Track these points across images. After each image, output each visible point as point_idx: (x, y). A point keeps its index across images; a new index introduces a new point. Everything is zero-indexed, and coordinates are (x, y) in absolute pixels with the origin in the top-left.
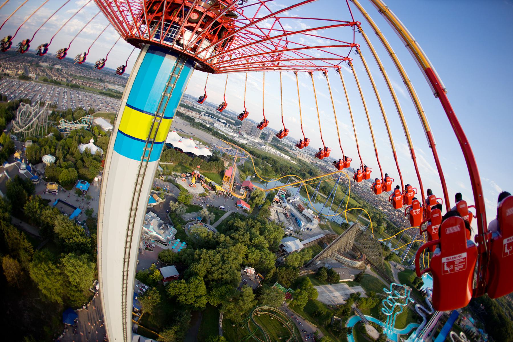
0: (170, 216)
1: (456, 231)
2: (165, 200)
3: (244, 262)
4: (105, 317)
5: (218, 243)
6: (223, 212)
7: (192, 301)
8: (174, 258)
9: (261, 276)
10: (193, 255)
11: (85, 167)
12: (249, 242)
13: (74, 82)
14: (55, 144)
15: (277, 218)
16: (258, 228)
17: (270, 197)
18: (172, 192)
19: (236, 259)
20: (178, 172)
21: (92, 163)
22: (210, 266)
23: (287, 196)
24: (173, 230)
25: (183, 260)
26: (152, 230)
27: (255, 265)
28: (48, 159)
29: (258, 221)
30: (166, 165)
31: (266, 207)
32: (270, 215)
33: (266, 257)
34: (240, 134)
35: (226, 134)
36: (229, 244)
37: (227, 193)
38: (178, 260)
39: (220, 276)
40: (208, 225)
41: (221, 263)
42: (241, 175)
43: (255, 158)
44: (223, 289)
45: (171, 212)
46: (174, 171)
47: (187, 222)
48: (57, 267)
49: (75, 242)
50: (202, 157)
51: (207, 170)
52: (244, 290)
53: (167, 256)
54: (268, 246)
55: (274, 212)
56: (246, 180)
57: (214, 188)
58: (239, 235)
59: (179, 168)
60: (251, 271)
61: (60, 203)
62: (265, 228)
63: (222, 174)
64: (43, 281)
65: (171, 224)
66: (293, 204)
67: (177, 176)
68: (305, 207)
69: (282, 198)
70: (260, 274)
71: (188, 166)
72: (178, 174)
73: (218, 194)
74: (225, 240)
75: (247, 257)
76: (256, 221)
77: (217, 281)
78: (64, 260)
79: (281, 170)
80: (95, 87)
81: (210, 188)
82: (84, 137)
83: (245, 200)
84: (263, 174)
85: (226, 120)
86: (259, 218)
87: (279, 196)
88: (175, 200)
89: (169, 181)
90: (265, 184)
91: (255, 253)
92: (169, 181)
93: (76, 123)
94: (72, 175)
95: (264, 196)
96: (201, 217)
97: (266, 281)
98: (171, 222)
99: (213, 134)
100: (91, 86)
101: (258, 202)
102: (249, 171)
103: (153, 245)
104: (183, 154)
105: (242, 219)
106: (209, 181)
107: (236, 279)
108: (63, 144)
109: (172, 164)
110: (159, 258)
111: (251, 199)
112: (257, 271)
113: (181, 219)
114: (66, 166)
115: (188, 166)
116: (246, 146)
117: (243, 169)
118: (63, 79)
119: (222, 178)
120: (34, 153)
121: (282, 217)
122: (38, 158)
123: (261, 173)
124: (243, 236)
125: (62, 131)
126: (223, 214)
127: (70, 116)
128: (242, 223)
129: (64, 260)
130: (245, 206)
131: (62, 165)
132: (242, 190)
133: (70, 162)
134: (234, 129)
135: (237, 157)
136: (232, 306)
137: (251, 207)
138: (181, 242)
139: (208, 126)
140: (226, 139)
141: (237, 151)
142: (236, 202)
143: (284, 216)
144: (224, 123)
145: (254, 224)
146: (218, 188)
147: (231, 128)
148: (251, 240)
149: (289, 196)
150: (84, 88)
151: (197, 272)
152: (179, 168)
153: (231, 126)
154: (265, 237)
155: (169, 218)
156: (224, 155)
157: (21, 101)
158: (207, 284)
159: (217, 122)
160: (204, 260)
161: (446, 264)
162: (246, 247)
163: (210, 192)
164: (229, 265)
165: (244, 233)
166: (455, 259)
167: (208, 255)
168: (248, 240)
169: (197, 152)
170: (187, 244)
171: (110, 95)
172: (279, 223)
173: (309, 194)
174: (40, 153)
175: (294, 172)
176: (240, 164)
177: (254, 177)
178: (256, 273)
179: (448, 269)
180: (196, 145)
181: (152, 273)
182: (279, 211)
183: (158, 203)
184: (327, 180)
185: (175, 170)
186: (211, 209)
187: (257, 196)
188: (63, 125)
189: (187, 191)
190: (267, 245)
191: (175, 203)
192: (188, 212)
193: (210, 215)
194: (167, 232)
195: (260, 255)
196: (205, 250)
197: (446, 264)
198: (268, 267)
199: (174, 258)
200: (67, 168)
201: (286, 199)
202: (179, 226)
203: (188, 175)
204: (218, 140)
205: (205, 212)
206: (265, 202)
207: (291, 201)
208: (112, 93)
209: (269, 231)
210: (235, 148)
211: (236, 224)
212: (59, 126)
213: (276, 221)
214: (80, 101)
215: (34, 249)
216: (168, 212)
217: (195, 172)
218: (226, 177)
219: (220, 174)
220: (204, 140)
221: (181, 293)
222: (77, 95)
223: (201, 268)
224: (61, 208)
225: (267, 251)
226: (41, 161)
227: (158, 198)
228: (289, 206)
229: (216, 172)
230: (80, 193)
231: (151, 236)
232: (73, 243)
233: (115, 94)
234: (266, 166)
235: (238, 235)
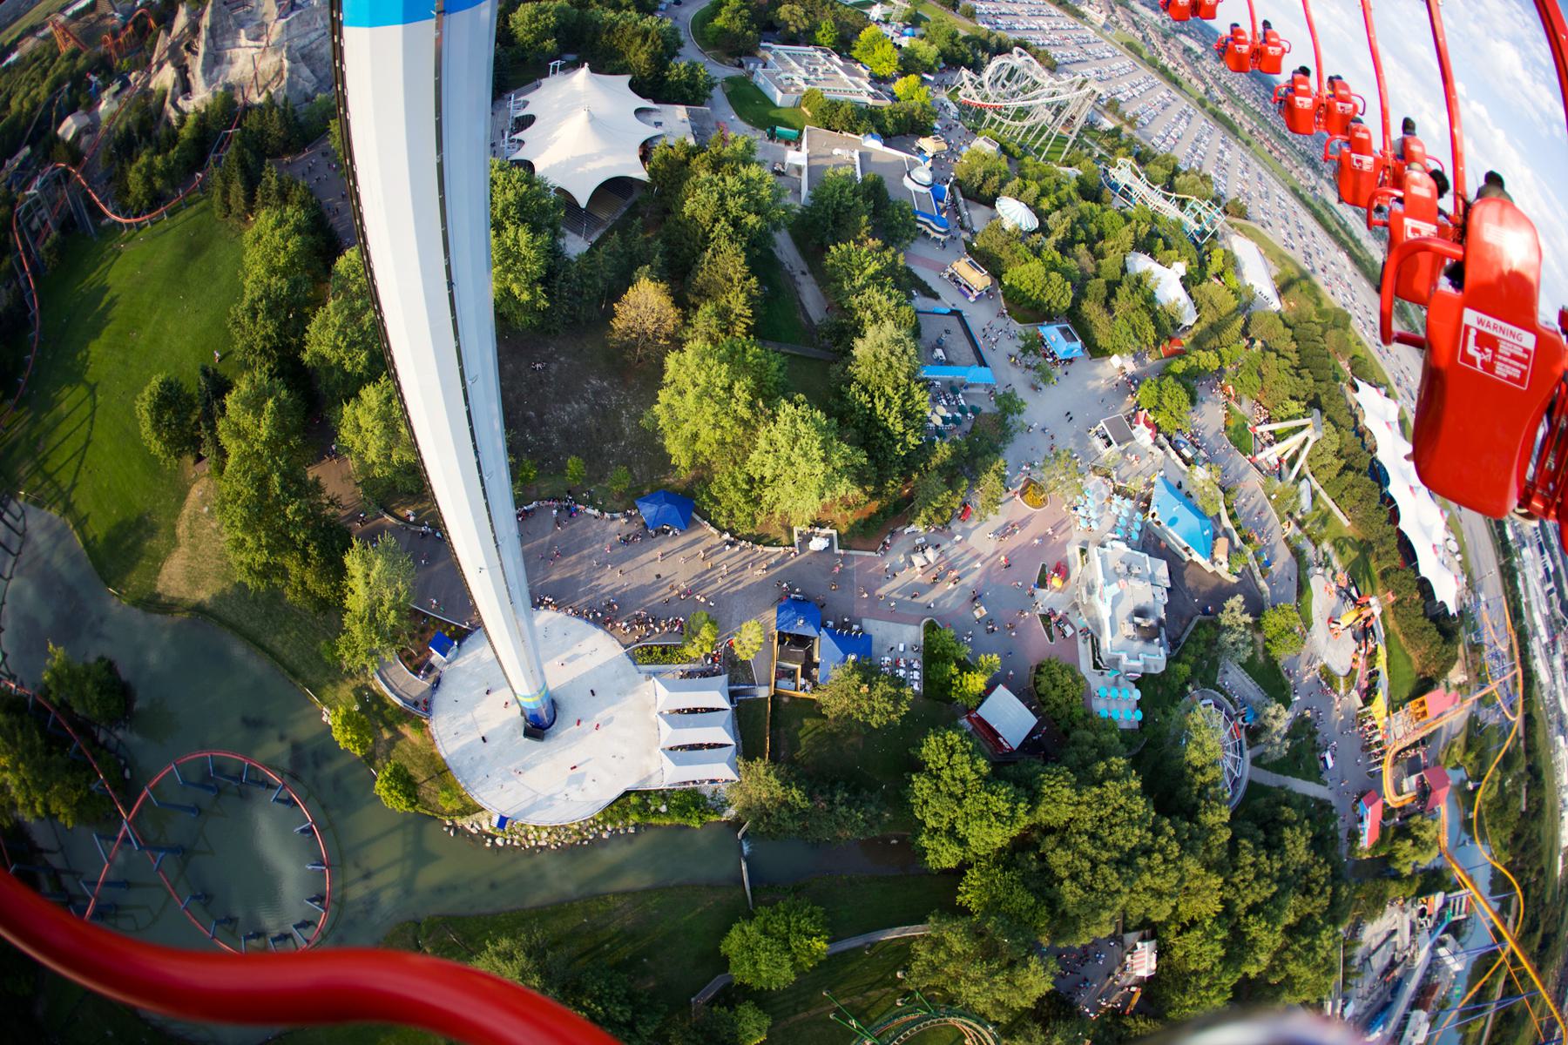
0: (1200, 625)
2: (1234, 580)
3: (1164, 925)
5: (1191, 813)
6: (1315, 773)
7: (931, 823)
8: (1066, 709)
9: (1135, 1001)
10: (1103, 755)
11: (1108, 308)
12: (1241, 907)
13: (1226, 110)
14: (1065, 199)
15: (1373, 947)
16: (1308, 910)
17: (1433, 880)
18: (1270, 584)
19: (1159, 894)
20: (1341, 560)
21: (1133, 316)
22: (1088, 826)
23: (1455, 929)
24: (1156, 658)
25: (1072, 735)
26: (1109, 600)
27: (1169, 966)
28: (1014, 213)
29: (1335, 893)
30: (1330, 512)
31: (1394, 889)
32: (1372, 917)
33: (1208, 988)
34: (1554, 642)
35: (1528, 605)
36: (1208, 850)
37: (1379, 744)
38: (1064, 724)
39: (1064, 873)
40: (1247, 754)
41: (1116, 854)
42: (1453, 744)
43: (1522, 744)
44: (1023, 899)
45: (1212, 623)
46: (1334, 544)
47: (1217, 688)
48: (751, 405)
49: (873, 409)
50: (1425, 587)
51: (1405, 635)
52: (1033, 966)
53: (1055, 686)
54: (1252, 975)
55: (1391, 926)
56: (1448, 770)
57: (1368, 696)
58: (1253, 865)
59: (1352, 554)
60: (1144, 962)
61: (954, 320)
62: (1315, 932)
63: (1425, 685)
64: (681, 393)
65: (1173, 643)
66: (1434, 964)
67: (1328, 564)
68: (1432, 1006)
69: (1441, 916)
70: (1138, 995)
71: (1376, 573)
72: (1335, 561)
73: (1359, 719)
74: (1212, 830)
75: (1185, 928)
76: (1329, 889)
77: (1046, 871)
78: (786, 409)
79: (1524, 849)
80: (1285, 164)
81: (1365, 685)
82: (1168, 247)
83: (1388, 812)
84: (1490, 804)
85: (1557, 569)
86: (1344, 891)
87: (1446, 904)
88: (1256, 607)
89: (1297, 554)
90: (1464, 836)
91: (1207, 947)
92: (1297, 554)
93: (1167, 198)
94: (1050, 295)
95: (1427, 860)
96: (1256, 716)
97: (1119, 1024)
98: (1183, 640)
99: (1501, 568)
100: (1275, 154)
101: (1400, 855)
102: (1477, 757)
103: (1069, 631)
104: (1389, 528)
105: (1321, 843)
106: (1381, 664)
107: (1078, 928)
108: (1087, 212)
109: (1347, 523)
110: (1039, 669)
111: (1400, 826)
112: (1145, 983)
113: (1214, 665)
114: (1053, 262)
115: (1376, 573)
116: (1536, 688)
117: (1475, 733)
118: (1195, 81)
119: (1411, 698)
120: (979, 171)
121: (1378, 962)
122: (987, 191)
123: (1489, 798)
124: (1257, 878)
125: (1115, 186)
126: (1307, 777)
127: (1161, 173)
128: (1301, 849)
129: (786, 409)
130: (1367, 824)
131: (1045, 254)
132: (1414, 778)
133: (1071, 263)
134: (1552, 613)
135: (1493, 686)
136: (958, 948)
137: (1376, 846)
138: (1139, 704)
139: (1510, 535)
140: (1516, 614)
141: (1508, 677)
142: (1369, 790)
143: (1386, 962)
144: (1546, 570)
145: (1317, 890)
146: (1380, 703)
147: (1550, 604)
148: (1254, 909)
149: (1457, 936)
150: (1248, 143)
151: (1043, 795)
152: (1352, 554)
153: (1554, 595)
154: (1286, 948)
155: (1191, 627)
156: (1476, 648)
157: (1024, 45)
158: (1022, 844)
159: (1536, 549)
160: (1101, 797)
162: (1219, 908)
163: (1354, 693)
164: (1119, 885)
165: (1269, 876)
167: (1122, 800)
168: (1249, 901)
169: (1428, 566)
170: (1142, 723)
171: (1318, 217)
172: (1357, 961)
173: (1482, 988)
174: (1002, 184)
175: (1532, 891)
176: (1483, 714)
177: (1470, 786)
178: (1141, 982)
180: (1439, 542)
181: (966, 667)
182: (1396, 938)
183: (1210, 568)
184: (1533, 1015)
185: (1339, 544)
186: (1303, 730)
187: (1416, 840)
188: (1123, 173)
189: (1308, 623)
190: (1253, 971)
191: (1245, 612)
192: (1248, 666)
193: (1278, 740)
194: (1138, 645)
195: (1207, 964)
196: (1136, 784)
198: (1171, 1009)
199: (1066, 709)
200: (1052, 267)
201: (1444, 932)
202: (1184, 669)
203: (1353, 591)
204: (1501, 592)
205: (1280, 719)
206: (1410, 878)
207: (1442, 951)
208: (1327, 216)
209: (1311, 948)
210: (1512, 659)
211: (1287, 833)
212: (1111, 171)
213: (1359, 951)
214: (1223, 167)
215: (749, 330)
216: (1205, 612)
217: (1373, 601)
218: (1423, 703)
219: (1420, 682)
220: (1471, 556)
221: (938, 777)
222: (1222, 146)
223: (1061, 802)
224: (947, 332)
225: (1229, 980)
226: (990, 202)
227: (1221, 556)
228: (1422, 957)
229: (1417, 664)
230: (1035, 346)
231: (1091, 606)
232: (862, 407)
233: (1335, 227)
234: (1517, 795)
235: (1250, 859)
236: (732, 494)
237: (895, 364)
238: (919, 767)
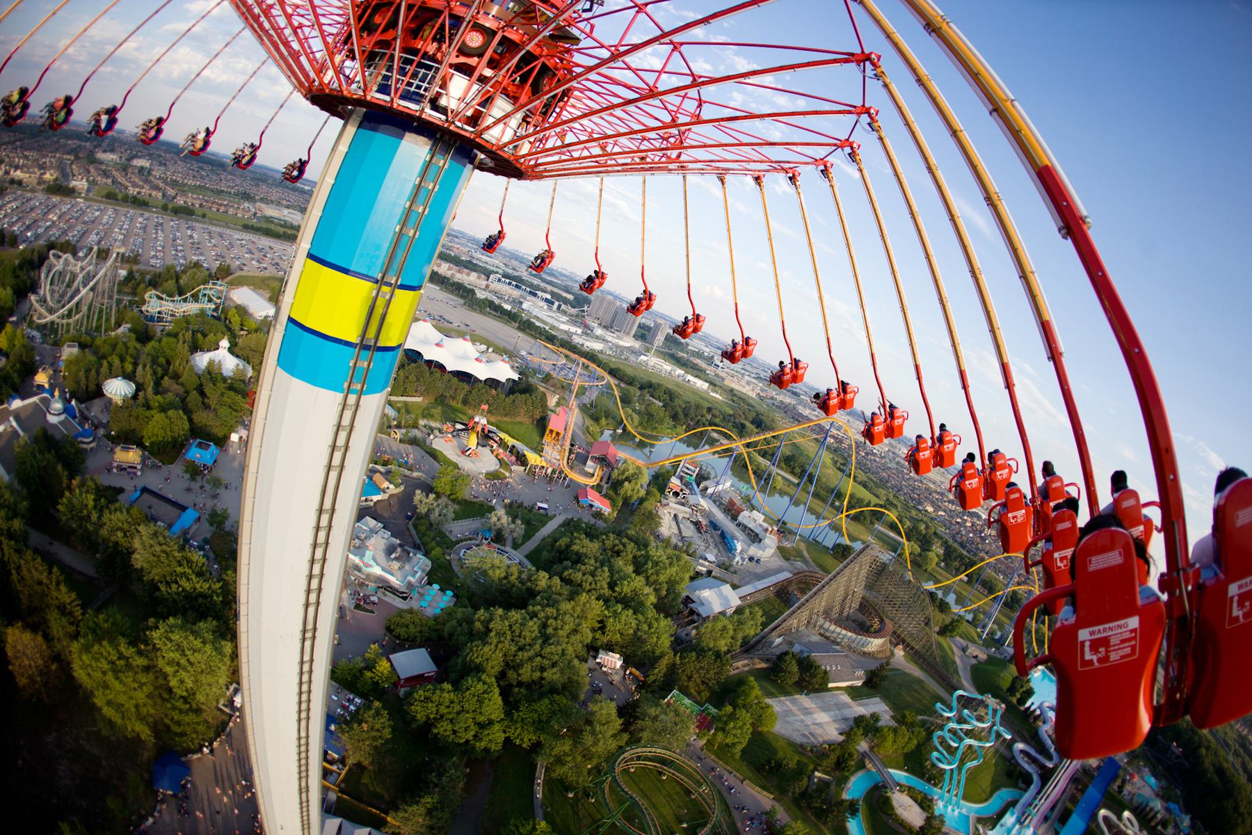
0: (415, 526)
2: (402, 488)
3: (594, 639)
4: (256, 774)
5: (532, 594)
6: (545, 517)
7: (470, 735)
8: (426, 629)
9: (637, 673)
10: (470, 622)
11: (207, 407)
12: (607, 592)
13: (180, 201)
14: (135, 352)
15: (676, 531)
16: (630, 556)
17: (660, 481)
18: (419, 470)
19: (575, 631)
20: (435, 420)
21: (225, 399)
22: (514, 648)
23: (701, 478)
24: (421, 563)
25: (446, 634)
26: (372, 563)
27: (622, 647)
29: (630, 539)
30: (406, 403)
31: (648, 505)
32: (658, 524)
33: (650, 626)
34: (586, 326)
35: (553, 327)
36: (560, 595)
37: (554, 472)
38: (434, 636)
39: (538, 674)
40: (508, 549)
41: (540, 641)
42: (587, 428)
43: (623, 385)
44: (544, 705)
45: (418, 518)
46: (424, 417)
47: (458, 542)
48: (140, 653)
49: (184, 590)
50: (492, 383)
51: (506, 415)
52: (596, 709)
53: (407, 626)
54: (655, 601)
55: (670, 518)
56: (601, 439)
57: (522, 460)
58: (584, 574)
59: (437, 411)
60: (613, 661)
62: (647, 557)
63: (542, 424)
64: (106, 686)
65: (417, 547)
66: (716, 499)
67: (432, 429)
68: (743, 506)
69: (687, 484)
70: (634, 670)
71: (459, 406)
72: (433, 424)
73: (532, 473)
74: (550, 587)
75: (602, 628)
76: (625, 540)
77: (530, 686)
78: (155, 635)
79: (686, 416)
80: (231, 211)
81: (514, 458)
82: (205, 335)
83: (598, 488)
84: (641, 424)
85: (552, 293)
86: (631, 532)
87: (681, 478)
88: (428, 489)
89: (414, 442)
90: (647, 450)
91: (623, 618)
92: (414, 442)
93: (185, 300)
94: (176, 428)
95: (645, 479)
96: (490, 530)
97: (649, 686)
98: (418, 542)
99: (519, 328)
100: (222, 209)
101: (629, 493)
102: (607, 417)
103: (374, 599)
104: (446, 377)
105: (591, 534)
106: (511, 441)
107: (577, 682)
108: (153, 352)
109: (420, 399)
110: (389, 629)
111: (613, 485)
112: (627, 663)
113: (442, 535)
114: (160, 405)
115: (459, 406)
116: (600, 356)
117: (594, 413)
118: (154, 193)
119: (542, 436)
121: (689, 531)
123: (636, 423)
124: (593, 576)
125: (152, 319)
126: (544, 524)
127: (171, 284)
128: (591, 545)
129: (155, 635)
130: (597, 504)
131: (151, 403)
132: (589, 463)
133: (170, 396)
134: (571, 315)
135: (577, 383)
136: (567, 748)
137: (613, 505)
138: (442, 590)
139: (507, 307)
140: (551, 339)
141: (579, 370)
142: (577, 493)
143: (692, 527)
144: (547, 300)
145: (621, 547)
146: (532, 458)
147: (565, 313)
148: (612, 586)
149: (706, 479)
150: (204, 216)
151: (480, 664)
152: (437, 411)
153: (563, 307)
154: (647, 578)
155: (413, 532)
156: (547, 378)
157: (52, 246)
158: (505, 693)
159: (530, 298)
160: (498, 634)
161: (1087, 644)
162: (601, 602)
163: (514, 468)
164: (560, 648)
165: (596, 569)
166: (1111, 633)
167: (507, 623)
168: (606, 586)
169: (481, 372)
170: (455, 595)
171: (268, 233)
172: (680, 544)
173: (754, 473)
175: (717, 420)
176: (586, 400)
177: (620, 431)
178: (625, 666)
179: (1095, 658)
180: (477, 355)
181: (370, 666)
182: (680, 516)
183: (386, 496)
184: (799, 440)
185: (427, 414)
186: (514, 510)
187: (628, 479)
188: (154, 304)
189: (456, 466)
190: (653, 599)
191: (427, 496)
192: (458, 517)
193: (513, 526)
194: (407, 567)
195: (634, 623)
196: (500, 611)
197: (1087, 644)
198: (653, 652)
199: (426, 629)
200: (163, 409)
201: (698, 485)
202: (437, 551)
203: (459, 426)
204: (532, 341)
205: (500, 517)
206: (648, 493)
207: (710, 491)
208: (272, 227)
209: (656, 564)
210: (573, 361)
211: (575, 548)
212: (144, 309)
213: (674, 540)
214: (196, 247)
216: (409, 518)
217: (477, 419)
218: (551, 431)
219: (537, 425)
220: (497, 342)
221: (442, 716)
222: (189, 232)
223: (491, 655)
225: (651, 613)
227: (386, 484)
228: (705, 504)
229: (526, 421)
230: (195, 471)
231: (368, 576)
232: (178, 594)
233: (281, 230)
234: (650, 404)
235: (580, 574)
236: (187, 719)
237: (168, 549)
238: (429, 724)
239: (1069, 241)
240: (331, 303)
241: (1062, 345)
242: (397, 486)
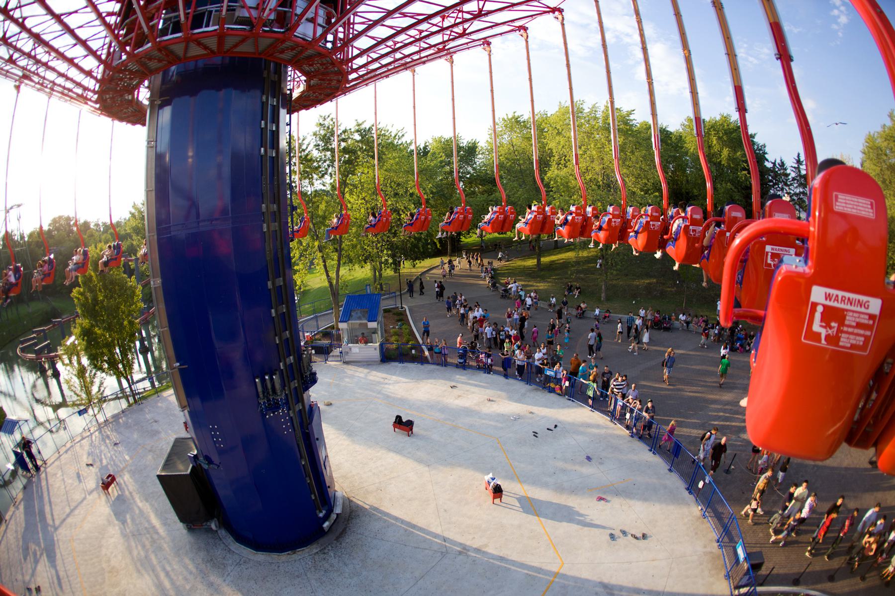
1: (849, 197)
4: (419, 365)
161: (820, 309)
166: (848, 307)
179: (823, 332)
197: (820, 309)
204: (422, 468)
239: (750, 132)
240: (389, 272)
241: (794, 49)
242: (419, 185)
